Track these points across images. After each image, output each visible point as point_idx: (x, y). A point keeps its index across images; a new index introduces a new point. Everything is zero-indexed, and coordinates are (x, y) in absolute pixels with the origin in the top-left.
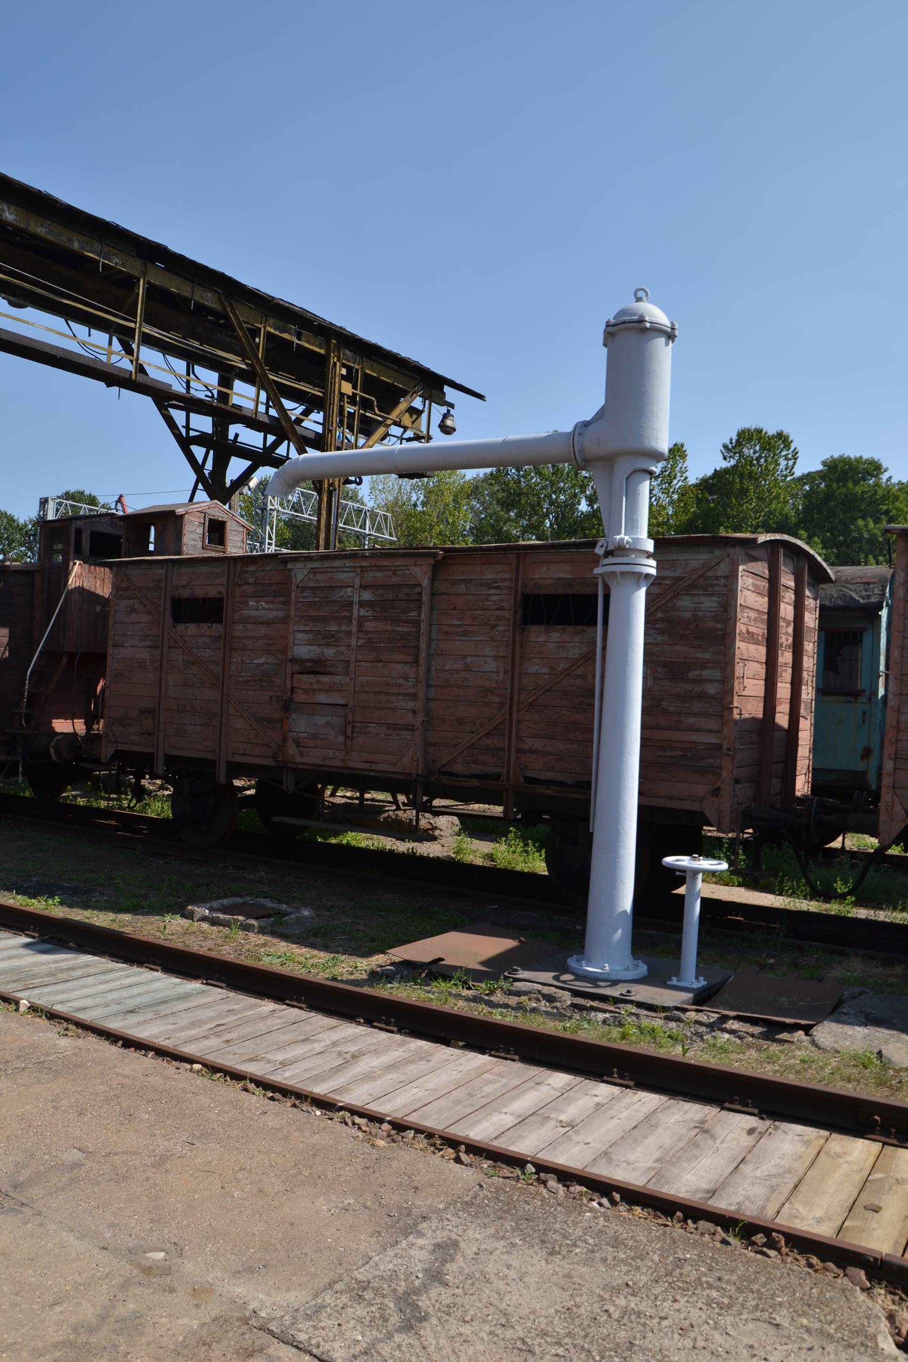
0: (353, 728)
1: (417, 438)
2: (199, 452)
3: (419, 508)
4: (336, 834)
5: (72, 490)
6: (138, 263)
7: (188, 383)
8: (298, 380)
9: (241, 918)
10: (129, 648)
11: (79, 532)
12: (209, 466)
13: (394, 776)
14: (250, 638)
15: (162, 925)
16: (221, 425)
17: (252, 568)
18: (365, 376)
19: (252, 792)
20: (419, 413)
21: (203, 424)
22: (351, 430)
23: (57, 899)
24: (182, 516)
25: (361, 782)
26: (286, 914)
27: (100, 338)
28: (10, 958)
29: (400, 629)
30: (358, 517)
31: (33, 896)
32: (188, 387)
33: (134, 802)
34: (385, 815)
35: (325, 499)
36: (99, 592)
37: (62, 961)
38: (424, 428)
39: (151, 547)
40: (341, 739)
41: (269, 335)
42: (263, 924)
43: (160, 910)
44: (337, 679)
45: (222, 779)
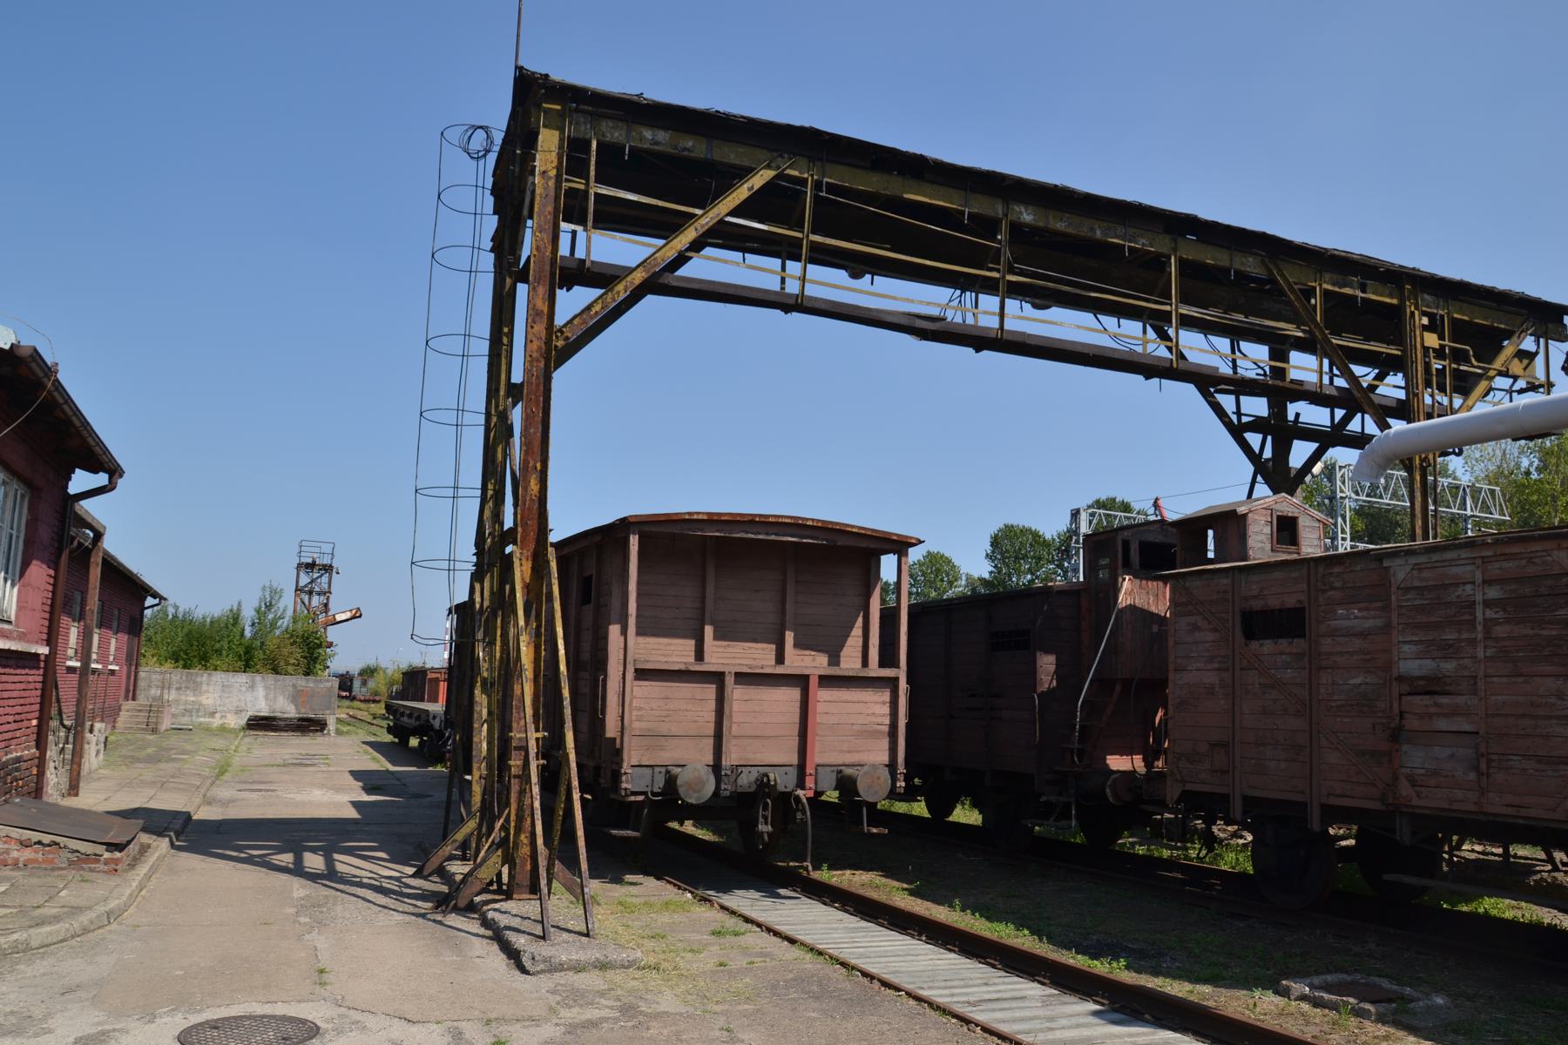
0: (1489, 762)
1: (1532, 387)
2: (1254, 439)
3: (1535, 476)
4: (1468, 901)
5: (1103, 497)
6: (1167, 239)
7: (1234, 361)
8: (1367, 339)
9: (1351, 1000)
10: (1194, 671)
11: (1126, 544)
12: (1268, 453)
13: (1552, 825)
14: (1341, 653)
15: (1251, 1001)
16: (1278, 408)
17: (1337, 570)
18: (1454, 321)
19: (1352, 842)
20: (1531, 356)
21: (1256, 406)
22: (1442, 389)
23: (1123, 962)
24: (1245, 516)
25: (1503, 832)
26: (1412, 1000)
27: (1132, 328)
28: (1078, 1026)
29: (1545, 633)
30: (1455, 496)
31: (1094, 957)
32: (1235, 367)
33: (1204, 852)
34: (1538, 877)
35: (1418, 478)
36: (1153, 609)
37: (1138, 1035)
38: (1540, 375)
39: (1211, 555)
40: (1472, 776)
41: (1326, 293)
42: (1381, 1010)
43: (1248, 983)
44: (1460, 700)
45: (1316, 826)
